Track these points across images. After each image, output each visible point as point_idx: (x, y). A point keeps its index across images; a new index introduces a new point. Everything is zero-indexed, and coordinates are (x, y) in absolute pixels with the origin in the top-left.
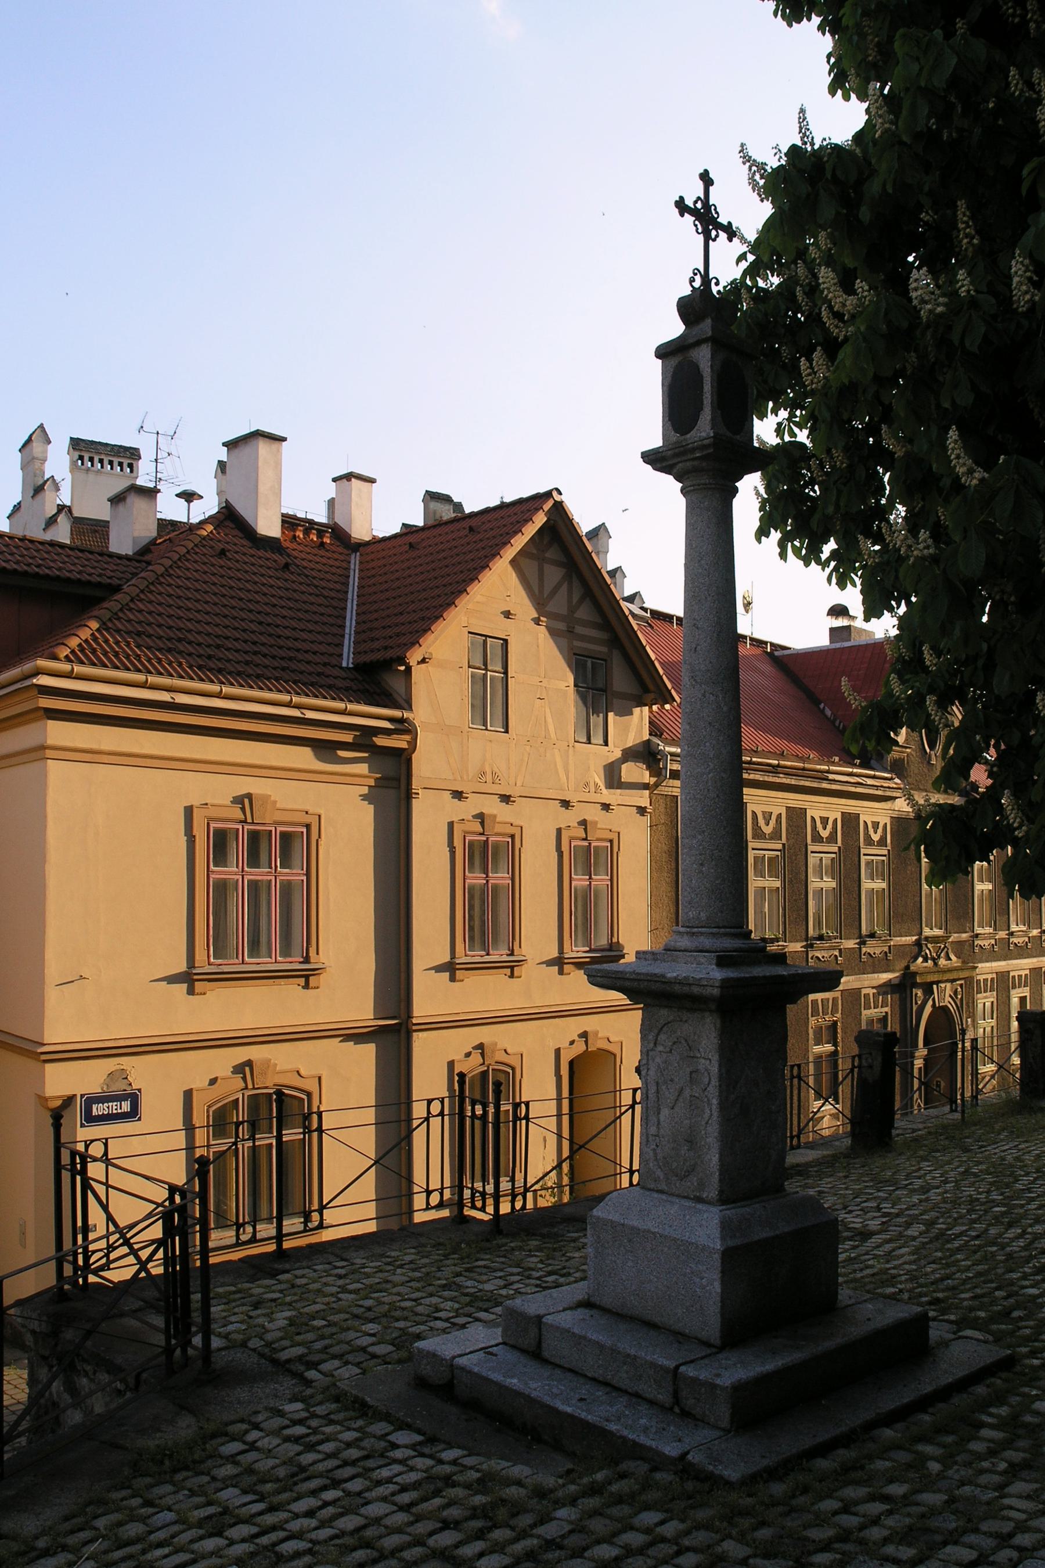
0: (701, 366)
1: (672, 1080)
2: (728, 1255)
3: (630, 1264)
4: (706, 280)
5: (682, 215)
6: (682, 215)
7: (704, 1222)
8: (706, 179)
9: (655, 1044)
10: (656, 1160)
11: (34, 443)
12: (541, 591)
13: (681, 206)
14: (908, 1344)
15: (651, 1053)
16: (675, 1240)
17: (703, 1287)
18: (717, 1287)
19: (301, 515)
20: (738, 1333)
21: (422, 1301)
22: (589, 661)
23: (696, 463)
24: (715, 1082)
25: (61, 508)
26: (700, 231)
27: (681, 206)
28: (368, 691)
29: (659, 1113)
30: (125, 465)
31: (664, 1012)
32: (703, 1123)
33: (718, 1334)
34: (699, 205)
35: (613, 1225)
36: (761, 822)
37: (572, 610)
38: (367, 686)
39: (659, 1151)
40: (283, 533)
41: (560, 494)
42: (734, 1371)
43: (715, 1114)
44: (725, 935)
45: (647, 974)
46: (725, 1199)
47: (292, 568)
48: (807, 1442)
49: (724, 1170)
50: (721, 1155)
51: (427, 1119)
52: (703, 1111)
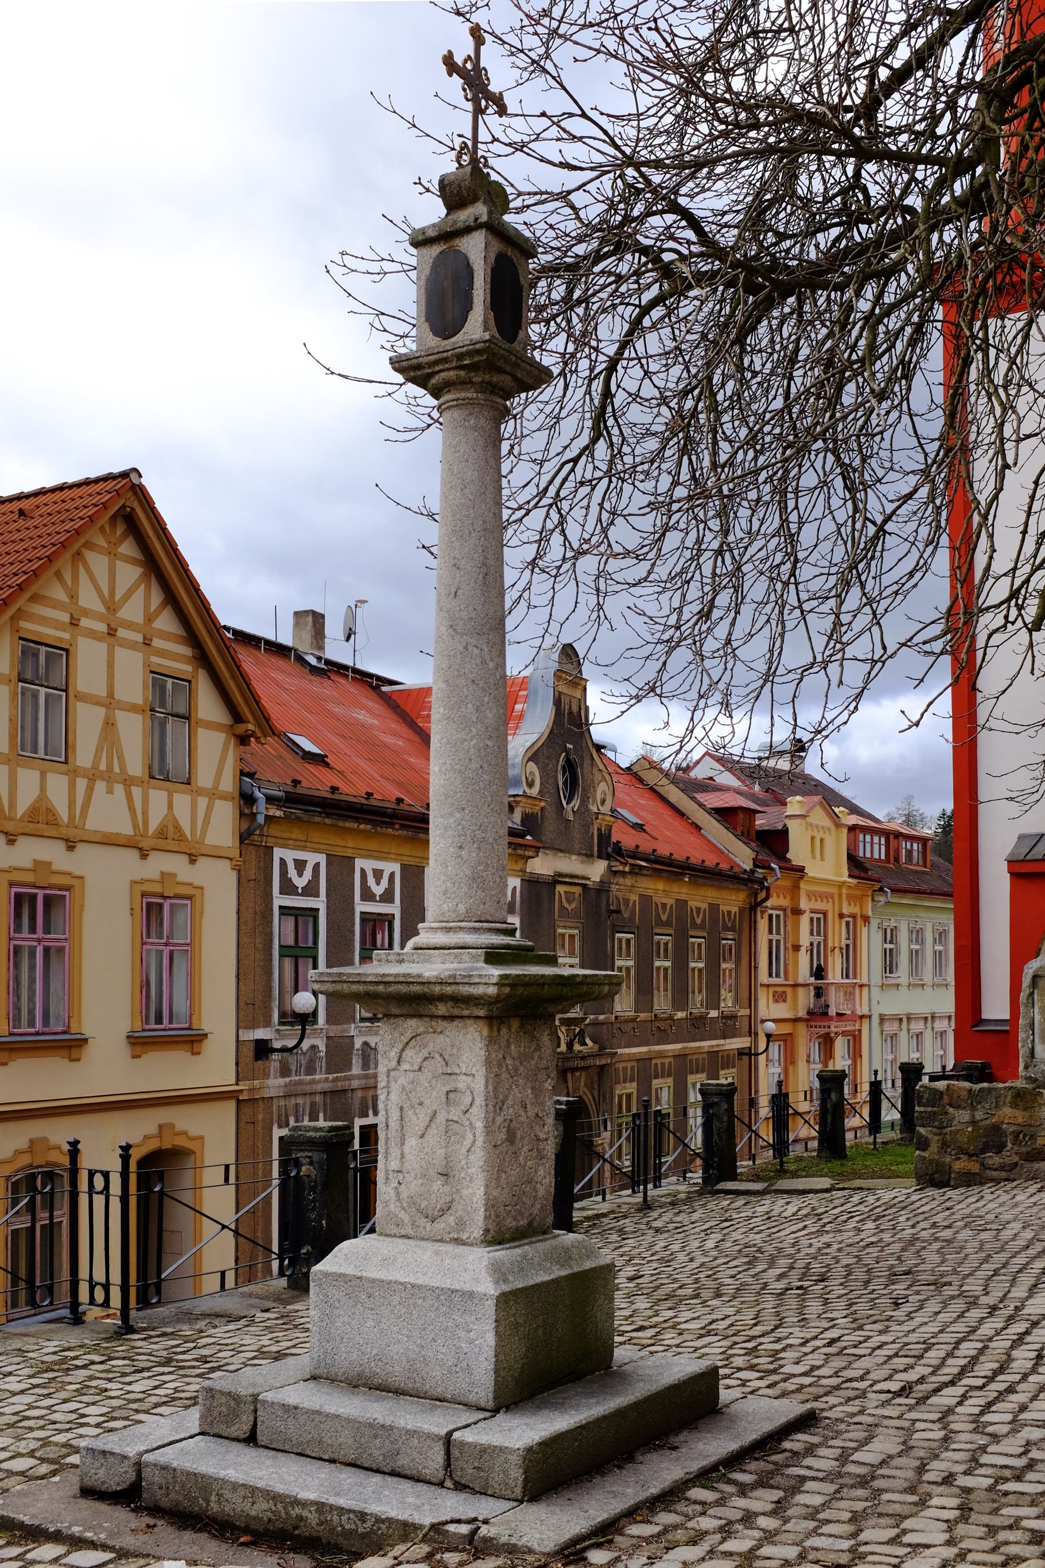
1: (421, 1104)
2: (504, 1300)
3: (370, 1323)
5: (450, 75)
6: (450, 75)
9: (399, 1062)
12: (112, 593)
15: (392, 1074)
16: (432, 1289)
17: (471, 1342)
18: (490, 1339)
20: (518, 1392)
21: (55, 1408)
22: (170, 681)
24: (479, 1101)
27: (449, 61)
29: (403, 1144)
31: (412, 1023)
32: (464, 1151)
33: (491, 1396)
34: (469, 66)
37: (149, 619)
41: (140, 476)
42: (523, 1432)
44: (490, 930)
46: (498, 1236)
48: (617, 1506)
49: (490, 1205)
50: (487, 1186)
52: (463, 1137)
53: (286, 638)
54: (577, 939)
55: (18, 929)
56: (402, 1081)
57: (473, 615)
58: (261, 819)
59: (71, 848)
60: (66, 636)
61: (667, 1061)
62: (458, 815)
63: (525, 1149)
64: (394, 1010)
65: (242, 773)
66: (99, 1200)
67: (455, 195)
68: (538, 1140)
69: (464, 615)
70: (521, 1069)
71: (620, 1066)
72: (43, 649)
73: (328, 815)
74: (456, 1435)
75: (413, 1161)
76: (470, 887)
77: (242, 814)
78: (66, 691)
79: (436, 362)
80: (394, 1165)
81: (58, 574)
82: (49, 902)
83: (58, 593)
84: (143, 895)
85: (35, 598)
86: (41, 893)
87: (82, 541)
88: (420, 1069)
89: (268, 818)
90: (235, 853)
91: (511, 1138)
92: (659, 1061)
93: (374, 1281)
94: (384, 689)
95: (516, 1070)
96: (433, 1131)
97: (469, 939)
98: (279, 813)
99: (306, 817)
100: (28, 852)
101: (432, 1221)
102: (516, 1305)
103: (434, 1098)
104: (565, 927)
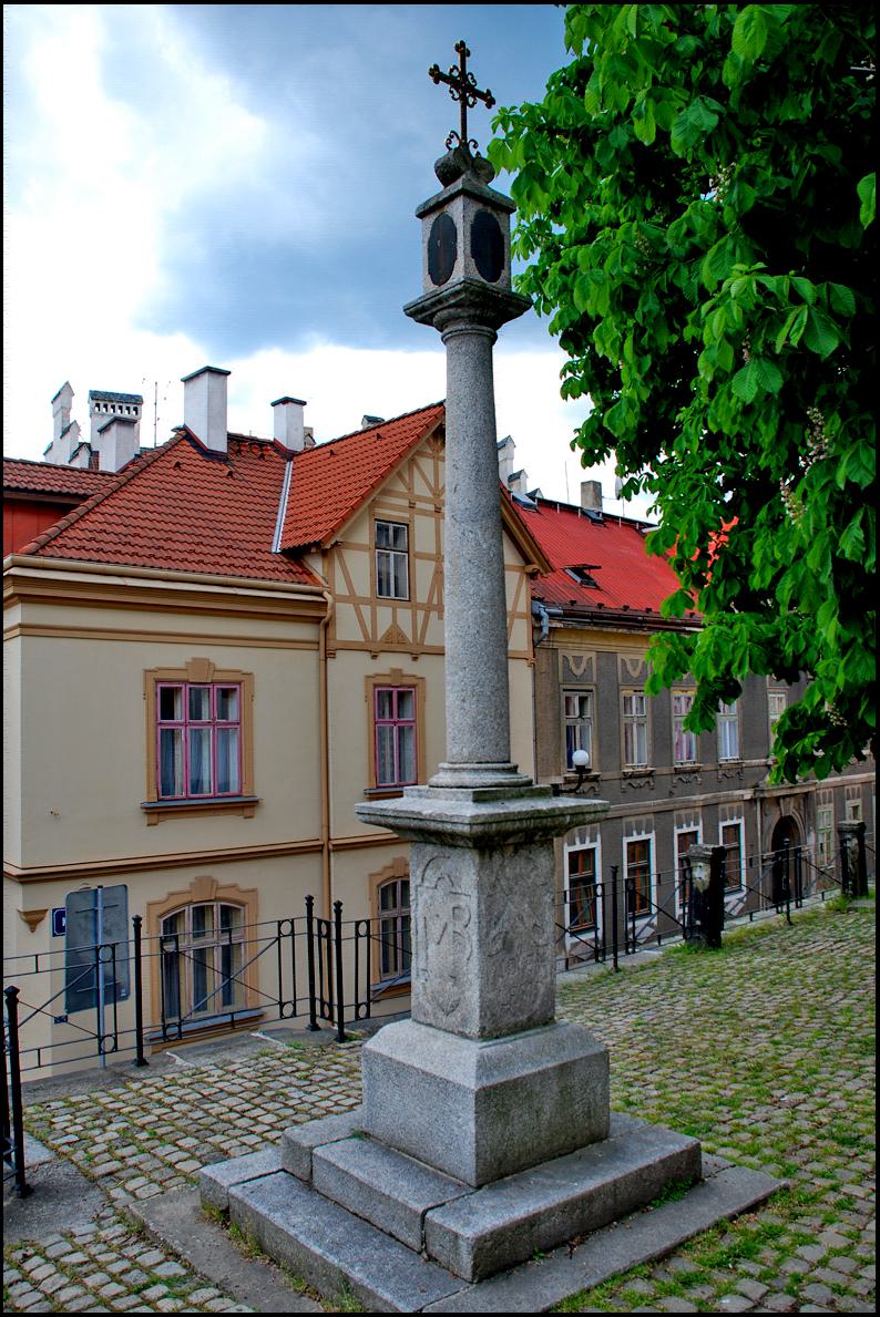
0: (455, 219)
1: (438, 916)
3: (397, 1098)
4: (464, 144)
7: (462, 1061)
8: (462, 50)
9: (423, 879)
10: (426, 994)
11: (64, 395)
13: (436, 75)
14: (683, 1177)
19: (246, 434)
23: (451, 310)
24: (474, 919)
25: (82, 445)
26: (457, 96)
27: (436, 75)
28: (291, 571)
30: (132, 409)
31: (429, 848)
33: (474, 1175)
35: (384, 1059)
36: (629, 667)
38: (292, 567)
39: (428, 984)
40: (229, 447)
43: (475, 950)
44: (487, 770)
45: (394, 811)
47: (183, 467)
50: (481, 991)
51: (278, 939)
53: (576, 501)
54: (784, 701)
55: (382, 715)
56: (425, 895)
57: (468, 506)
58: (546, 631)
59: (415, 659)
60: (407, 515)
61: (856, 787)
62: (461, 673)
63: (524, 955)
64: (415, 838)
65: (533, 598)
66: (324, 941)
67: (446, 173)
68: (538, 946)
69: (462, 506)
70: (517, 888)
71: (821, 792)
72: (391, 526)
73: (596, 624)
74: (429, 1214)
75: (434, 964)
76: (472, 735)
77: (534, 628)
78: (408, 552)
79: (433, 304)
80: (422, 965)
81: (400, 475)
82: (402, 696)
83: (401, 488)
84: (375, 686)
85: (386, 492)
86: (395, 691)
87: (414, 451)
88: (436, 887)
89: (551, 629)
90: (531, 655)
91: (508, 946)
92: (850, 787)
93: (398, 1063)
94: (644, 531)
95: (510, 889)
96: (445, 940)
97: (467, 778)
98: (559, 625)
99: (579, 627)
100: (388, 663)
101: (445, 1017)
102: (494, 1100)
103: (446, 915)
104: (774, 693)
